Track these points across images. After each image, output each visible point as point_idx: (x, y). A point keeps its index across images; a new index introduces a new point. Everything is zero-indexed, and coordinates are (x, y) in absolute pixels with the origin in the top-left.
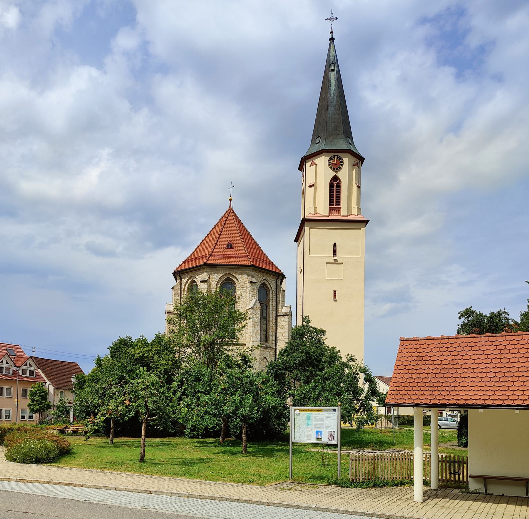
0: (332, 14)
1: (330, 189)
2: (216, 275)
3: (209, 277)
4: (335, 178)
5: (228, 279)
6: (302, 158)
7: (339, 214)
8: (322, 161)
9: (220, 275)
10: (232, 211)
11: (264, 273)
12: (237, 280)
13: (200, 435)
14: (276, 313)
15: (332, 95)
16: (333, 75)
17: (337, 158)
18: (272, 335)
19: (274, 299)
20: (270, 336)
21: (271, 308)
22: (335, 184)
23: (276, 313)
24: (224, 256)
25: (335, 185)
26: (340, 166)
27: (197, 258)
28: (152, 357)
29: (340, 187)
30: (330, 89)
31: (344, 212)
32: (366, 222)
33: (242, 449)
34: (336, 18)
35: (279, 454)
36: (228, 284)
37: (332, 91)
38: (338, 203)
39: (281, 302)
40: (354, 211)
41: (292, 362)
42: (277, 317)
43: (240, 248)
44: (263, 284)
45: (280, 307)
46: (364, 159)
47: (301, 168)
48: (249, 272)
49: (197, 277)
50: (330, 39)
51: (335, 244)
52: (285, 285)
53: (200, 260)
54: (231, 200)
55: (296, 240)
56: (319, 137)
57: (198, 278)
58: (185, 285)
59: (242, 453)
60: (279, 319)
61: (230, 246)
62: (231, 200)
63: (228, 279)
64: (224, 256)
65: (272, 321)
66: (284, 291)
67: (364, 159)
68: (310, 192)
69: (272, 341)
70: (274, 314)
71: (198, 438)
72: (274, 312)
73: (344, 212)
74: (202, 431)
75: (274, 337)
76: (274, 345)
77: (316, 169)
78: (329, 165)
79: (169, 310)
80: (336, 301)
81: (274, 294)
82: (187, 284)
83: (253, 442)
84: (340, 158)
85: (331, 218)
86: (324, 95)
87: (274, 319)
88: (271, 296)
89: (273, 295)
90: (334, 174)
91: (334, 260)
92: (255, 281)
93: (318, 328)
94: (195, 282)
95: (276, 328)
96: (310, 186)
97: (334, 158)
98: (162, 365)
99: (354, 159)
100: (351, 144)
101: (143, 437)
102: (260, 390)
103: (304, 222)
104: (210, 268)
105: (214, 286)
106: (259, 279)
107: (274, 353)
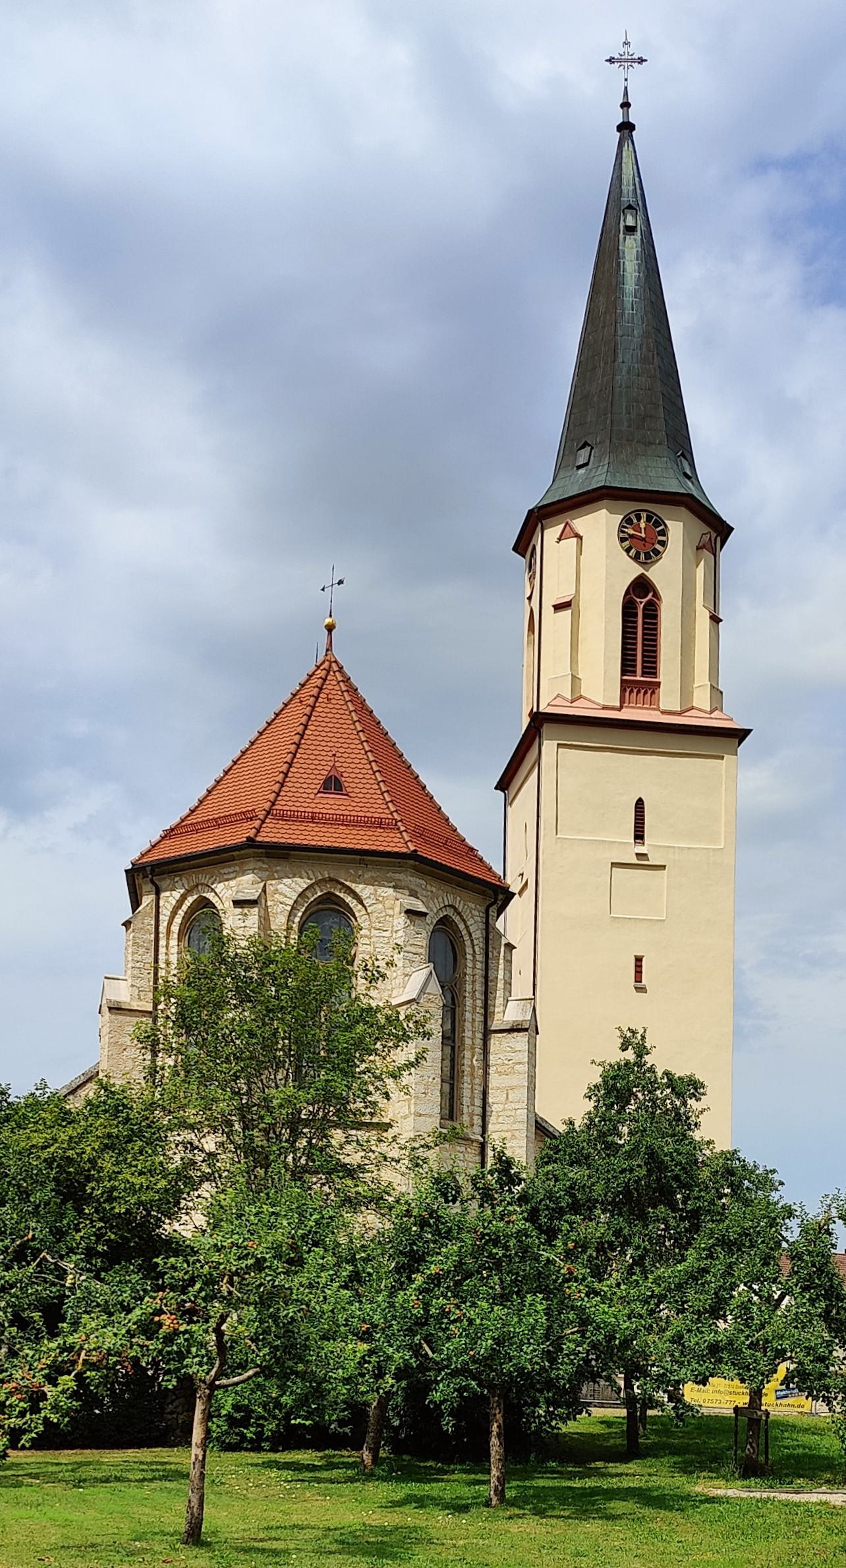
0: (626, 43)
1: (624, 621)
2: (287, 881)
3: (264, 890)
5: (329, 898)
7: (654, 704)
8: (600, 526)
9: (302, 883)
10: (335, 667)
12: (361, 902)
13: (267, 1439)
14: (485, 1022)
15: (628, 311)
16: (631, 246)
17: (649, 519)
18: (472, 1098)
19: (480, 973)
20: (466, 1101)
21: (469, 1002)
22: (641, 603)
23: (485, 1022)
24: (313, 818)
25: (640, 608)
26: (658, 547)
27: (218, 823)
28: (92, 1161)
29: (656, 617)
30: (622, 290)
32: (741, 735)
33: (488, 1491)
34: (641, 61)
35: (617, 1506)
36: (328, 915)
37: (629, 299)
38: (651, 667)
40: (702, 699)
41: (599, 1188)
43: (366, 794)
44: (444, 921)
45: (499, 1001)
46: (732, 529)
47: (524, 544)
48: (401, 876)
49: (219, 887)
50: (620, 128)
51: (640, 803)
52: (514, 922)
53: (228, 829)
55: (503, 784)
56: (585, 444)
57: (223, 893)
58: (174, 913)
59: (488, 1504)
60: (495, 1041)
61: (333, 784)
62: (330, 628)
63: (329, 898)
64: (313, 818)
65: (473, 1048)
66: (510, 947)
67: (732, 529)
68: (555, 626)
69: (471, 1115)
70: (479, 1026)
71: (257, 1448)
72: (479, 1018)
74: (273, 1426)
75: (478, 1102)
76: (478, 1130)
78: (622, 540)
79: (113, 998)
80: (641, 989)
81: (480, 958)
82: (181, 913)
83: (462, 1462)
84: (657, 522)
85: (627, 714)
86: (602, 309)
87: (479, 1042)
88: (470, 964)
89: (474, 960)
90: (636, 570)
92: (424, 909)
93: (680, 1071)
94: (208, 903)
95: (486, 1074)
96: (558, 608)
97: (639, 518)
98: (132, 1189)
99: (700, 528)
100: (689, 478)
101: (196, 1451)
102: (568, 1281)
103: (539, 721)
104: (268, 856)
105: (279, 921)
106: (434, 901)
107: (478, 1159)
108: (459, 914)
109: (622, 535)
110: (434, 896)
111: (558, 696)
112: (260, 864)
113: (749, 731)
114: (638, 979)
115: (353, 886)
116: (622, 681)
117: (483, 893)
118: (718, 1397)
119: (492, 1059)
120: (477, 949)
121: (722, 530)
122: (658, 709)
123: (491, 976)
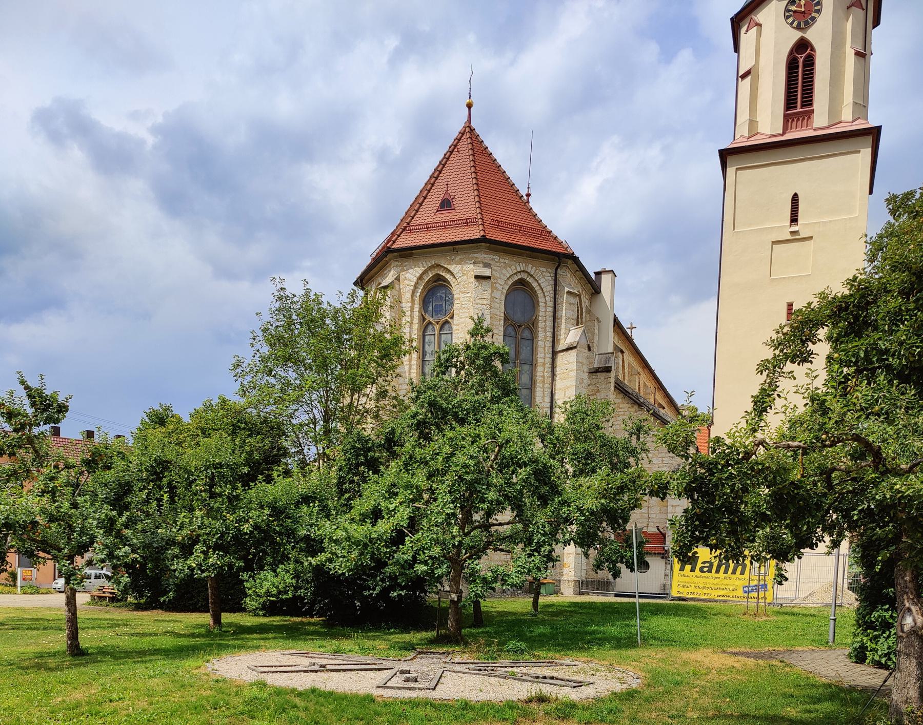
2: (411, 271)
4: (803, 46)
6: (732, 19)
9: (418, 271)
11: (520, 255)
12: (452, 274)
22: (801, 59)
23: (553, 347)
25: (800, 65)
26: (814, 14)
31: (820, 120)
38: (808, 100)
39: (563, 321)
40: (847, 114)
42: (554, 354)
48: (478, 255)
51: (795, 198)
54: (469, 106)
60: (561, 358)
62: (469, 106)
65: (544, 364)
73: (820, 120)
75: (548, 399)
77: (759, 34)
78: (787, 18)
85: (789, 136)
87: (549, 360)
91: (791, 232)
95: (553, 380)
104: (401, 257)
106: (506, 271)
108: (532, 276)
110: (506, 266)
112: (397, 263)
115: (449, 267)
116: (785, 116)
117: (553, 260)
118: (698, 590)
119: (558, 370)
120: (548, 298)
123: (558, 314)
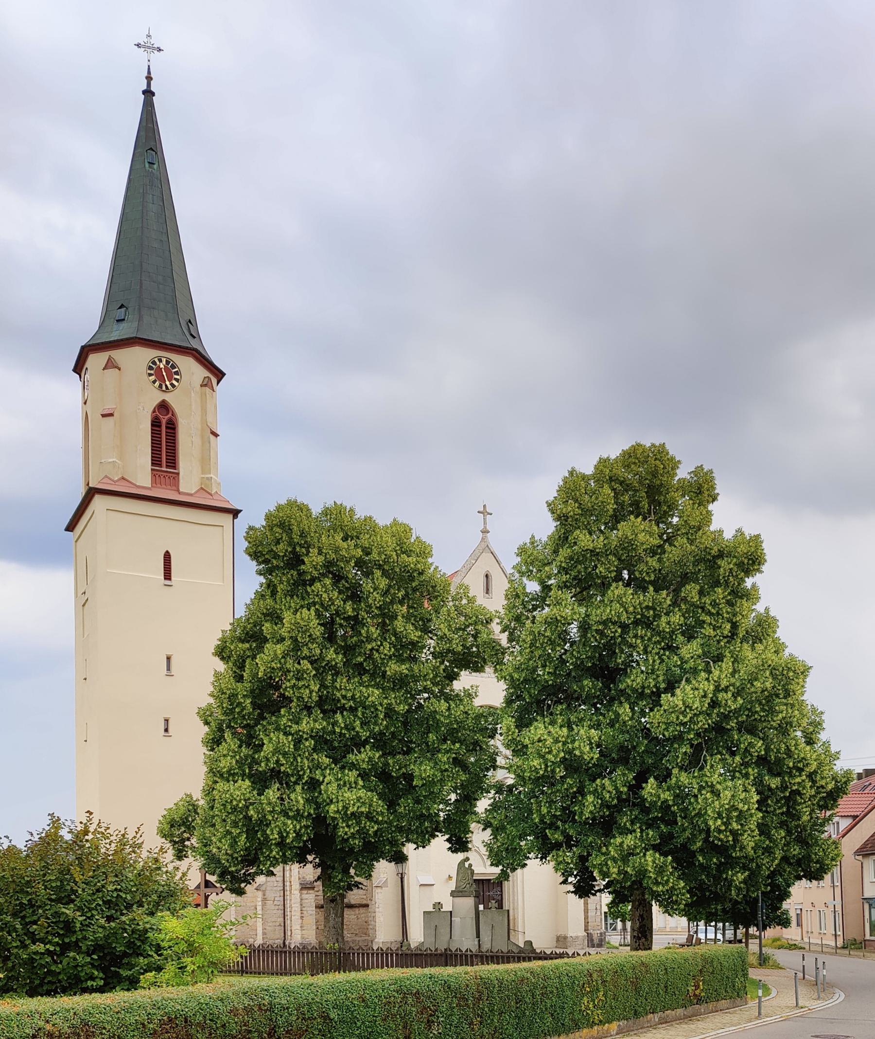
0: (149, 36)
8: (137, 359)
29: (174, 429)
38: (173, 462)
50: (144, 92)
51: (167, 557)
103: (91, 493)
109: (149, 372)
111: (106, 476)
113: (241, 511)
114: (169, 669)
121: (219, 375)
122: (178, 490)
